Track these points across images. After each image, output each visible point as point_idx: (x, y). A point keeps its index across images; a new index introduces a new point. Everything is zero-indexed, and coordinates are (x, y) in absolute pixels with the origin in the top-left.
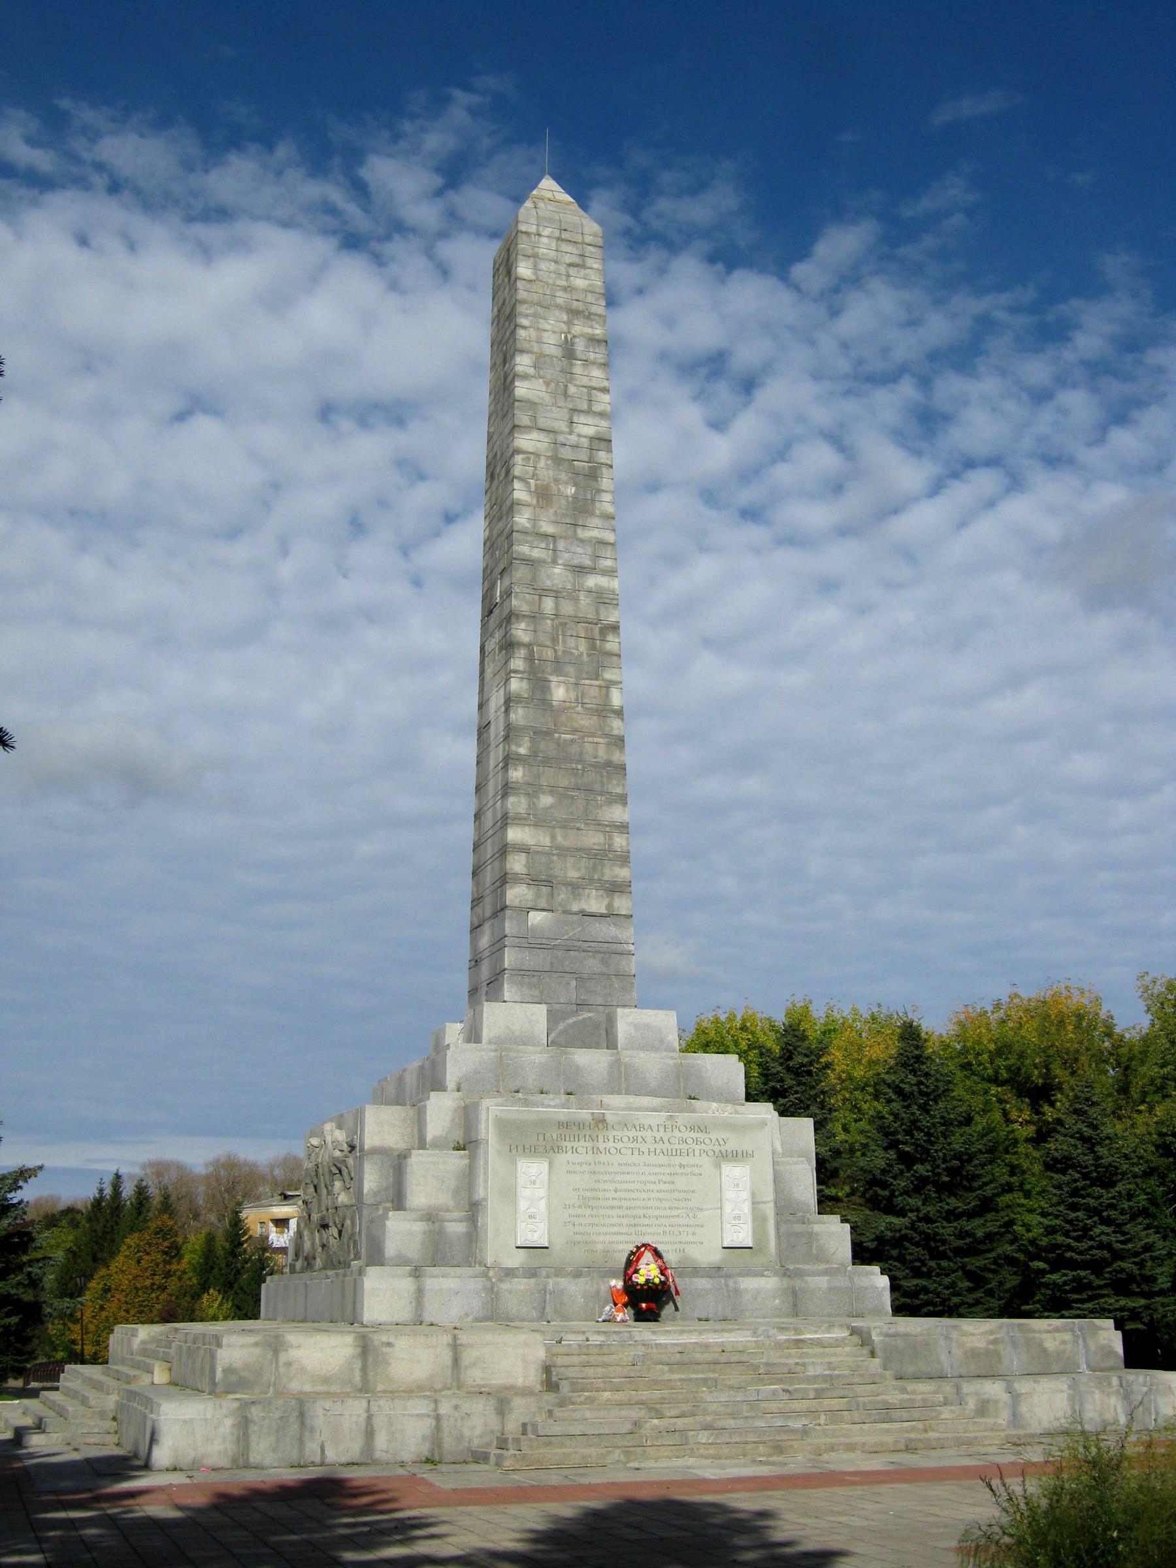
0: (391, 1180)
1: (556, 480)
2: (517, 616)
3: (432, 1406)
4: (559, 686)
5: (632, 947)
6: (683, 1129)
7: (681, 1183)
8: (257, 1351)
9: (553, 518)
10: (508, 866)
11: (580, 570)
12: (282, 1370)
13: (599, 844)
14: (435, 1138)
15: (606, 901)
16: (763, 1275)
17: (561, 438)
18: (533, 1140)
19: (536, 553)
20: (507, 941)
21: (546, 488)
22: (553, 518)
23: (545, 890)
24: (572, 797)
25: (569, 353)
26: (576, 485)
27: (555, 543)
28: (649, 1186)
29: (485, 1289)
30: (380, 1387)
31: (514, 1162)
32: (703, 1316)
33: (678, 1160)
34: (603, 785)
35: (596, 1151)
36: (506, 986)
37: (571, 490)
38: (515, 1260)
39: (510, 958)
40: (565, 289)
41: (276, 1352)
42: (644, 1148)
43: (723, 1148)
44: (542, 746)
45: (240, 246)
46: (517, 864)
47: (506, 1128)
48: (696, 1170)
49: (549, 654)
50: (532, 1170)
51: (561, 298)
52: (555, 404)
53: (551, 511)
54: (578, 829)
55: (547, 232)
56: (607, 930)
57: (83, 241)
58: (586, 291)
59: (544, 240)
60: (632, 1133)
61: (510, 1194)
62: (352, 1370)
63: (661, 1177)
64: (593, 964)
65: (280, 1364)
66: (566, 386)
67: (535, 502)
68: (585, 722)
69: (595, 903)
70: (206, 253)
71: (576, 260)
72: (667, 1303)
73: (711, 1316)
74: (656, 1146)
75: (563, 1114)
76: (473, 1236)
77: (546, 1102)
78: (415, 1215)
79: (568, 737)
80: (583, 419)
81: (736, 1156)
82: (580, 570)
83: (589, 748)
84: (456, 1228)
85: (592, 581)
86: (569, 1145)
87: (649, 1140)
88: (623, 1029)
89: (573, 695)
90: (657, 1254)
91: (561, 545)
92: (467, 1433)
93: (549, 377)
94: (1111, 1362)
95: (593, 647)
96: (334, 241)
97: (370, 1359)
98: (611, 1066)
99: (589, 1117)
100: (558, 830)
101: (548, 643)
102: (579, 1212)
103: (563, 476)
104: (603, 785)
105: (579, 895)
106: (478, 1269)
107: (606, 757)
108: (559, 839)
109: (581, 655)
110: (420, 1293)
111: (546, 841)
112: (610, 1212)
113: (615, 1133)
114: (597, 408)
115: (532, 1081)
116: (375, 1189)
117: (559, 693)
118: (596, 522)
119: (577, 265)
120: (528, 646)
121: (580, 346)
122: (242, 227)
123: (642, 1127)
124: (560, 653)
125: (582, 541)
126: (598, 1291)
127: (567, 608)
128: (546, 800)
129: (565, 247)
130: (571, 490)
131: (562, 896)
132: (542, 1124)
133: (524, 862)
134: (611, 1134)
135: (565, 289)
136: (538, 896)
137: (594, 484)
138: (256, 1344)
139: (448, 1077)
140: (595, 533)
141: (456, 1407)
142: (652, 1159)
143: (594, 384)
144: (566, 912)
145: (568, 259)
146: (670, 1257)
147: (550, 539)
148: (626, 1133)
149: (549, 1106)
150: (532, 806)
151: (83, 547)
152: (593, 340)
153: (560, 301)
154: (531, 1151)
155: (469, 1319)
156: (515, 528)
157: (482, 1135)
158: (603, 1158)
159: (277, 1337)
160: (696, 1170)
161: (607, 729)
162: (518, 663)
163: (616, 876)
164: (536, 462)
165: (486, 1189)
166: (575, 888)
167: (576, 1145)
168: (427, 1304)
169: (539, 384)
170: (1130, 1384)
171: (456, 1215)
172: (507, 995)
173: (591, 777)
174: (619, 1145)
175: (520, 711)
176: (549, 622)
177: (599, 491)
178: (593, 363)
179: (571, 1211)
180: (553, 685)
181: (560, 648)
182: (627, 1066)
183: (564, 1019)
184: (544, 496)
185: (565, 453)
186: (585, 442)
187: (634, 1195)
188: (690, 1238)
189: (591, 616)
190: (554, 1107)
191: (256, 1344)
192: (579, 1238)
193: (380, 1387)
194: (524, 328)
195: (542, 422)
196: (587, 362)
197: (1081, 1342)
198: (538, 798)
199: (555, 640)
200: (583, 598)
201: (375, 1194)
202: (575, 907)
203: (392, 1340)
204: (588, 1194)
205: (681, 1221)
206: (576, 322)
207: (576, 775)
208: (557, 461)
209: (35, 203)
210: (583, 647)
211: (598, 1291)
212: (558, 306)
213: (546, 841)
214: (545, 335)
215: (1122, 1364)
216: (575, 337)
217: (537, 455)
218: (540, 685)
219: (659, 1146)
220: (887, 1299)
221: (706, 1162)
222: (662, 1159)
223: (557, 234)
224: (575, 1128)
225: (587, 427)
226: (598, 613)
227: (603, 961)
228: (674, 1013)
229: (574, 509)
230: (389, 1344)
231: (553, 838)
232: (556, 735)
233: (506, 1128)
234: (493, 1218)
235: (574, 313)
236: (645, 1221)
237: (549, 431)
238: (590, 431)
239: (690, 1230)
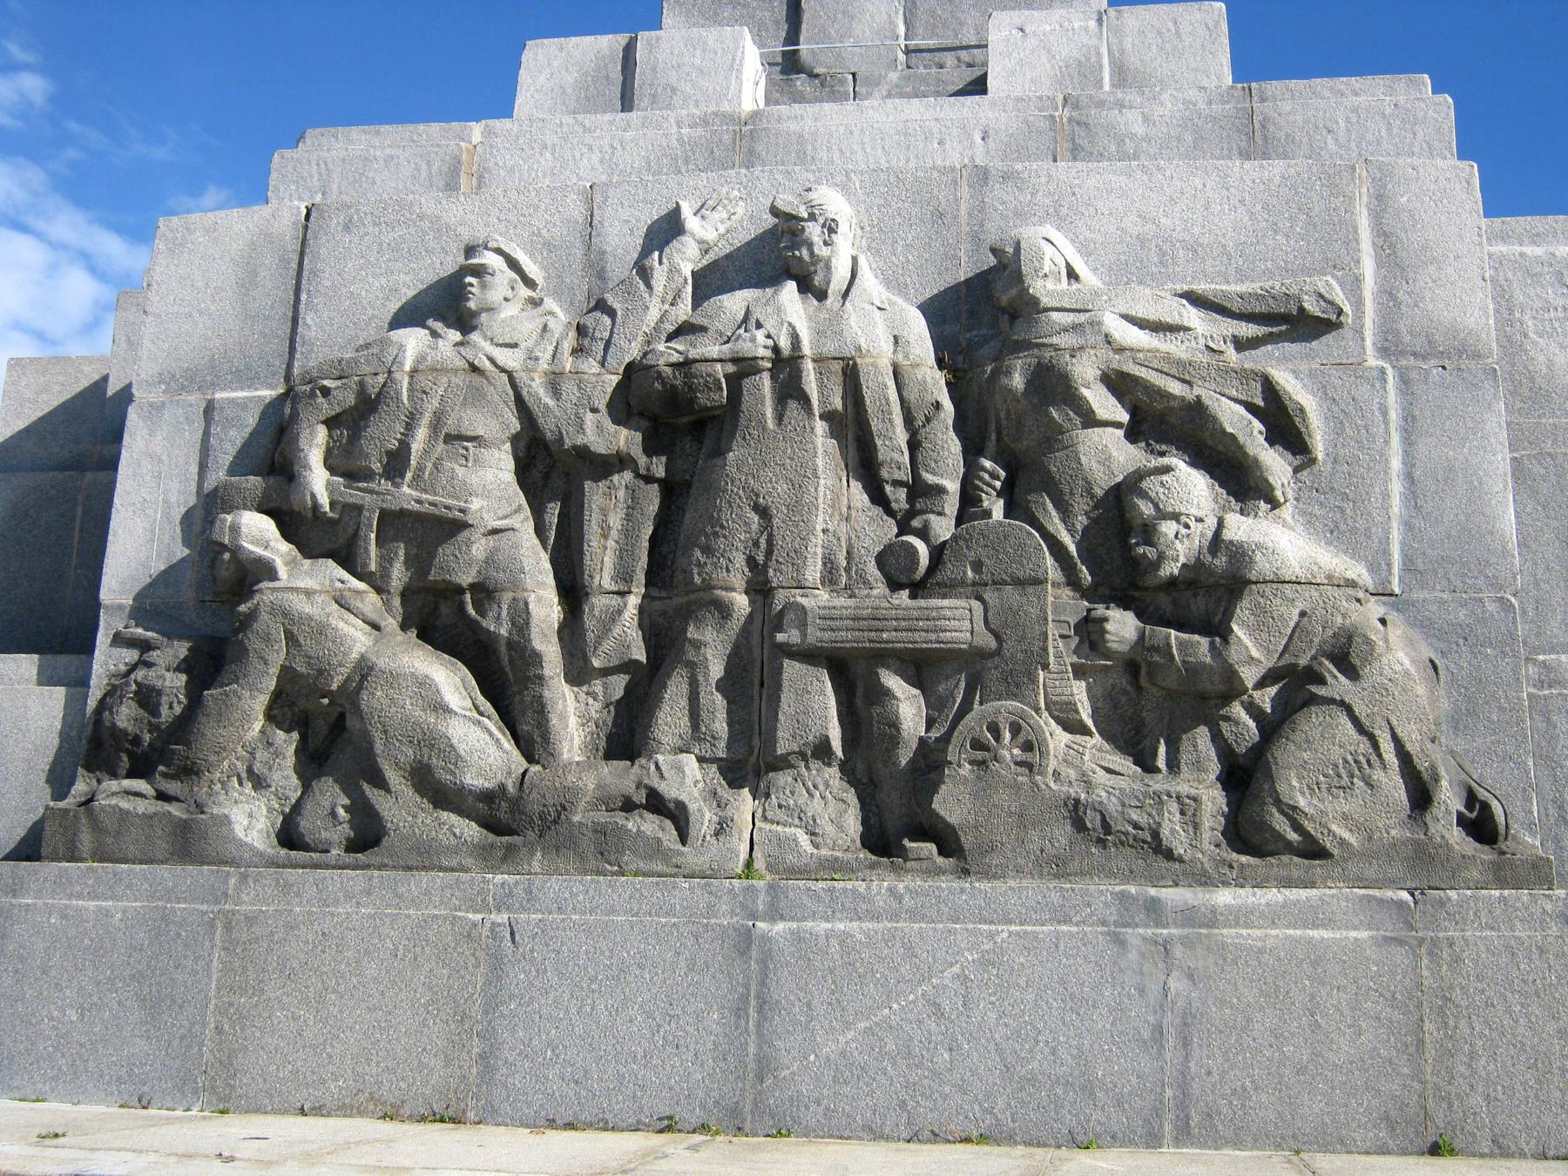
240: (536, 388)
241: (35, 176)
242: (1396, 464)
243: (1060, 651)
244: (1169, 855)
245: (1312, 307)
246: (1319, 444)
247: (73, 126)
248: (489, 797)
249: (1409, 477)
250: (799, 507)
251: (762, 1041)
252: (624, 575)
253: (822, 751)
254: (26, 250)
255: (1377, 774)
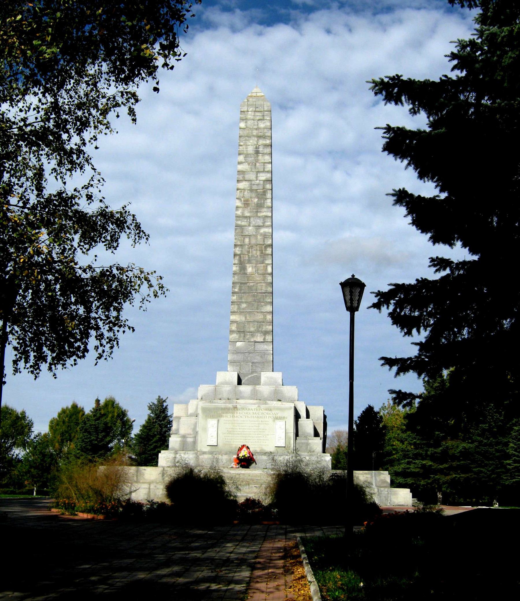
1: (251, 197)
3: (148, 486)
7: (262, 426)
9: (249, 210)
11: (258, 227)
15: (263, 337)
17: (253, 182)
19: (243, 224)
21: (247, 200)
23: (242, 335)
25: (257, 152)
26: (258, 198)
28: (251, 428)
30: (141, 481)
31: (206, 419)
33: (260, 420)
35: (233, 417)
37: (256, 200)
38: (207, 449)
40: (256, 129)
42: (249, 416)
44: (243, 288)
45: (400, 21)
48: (267, 423)
51: (255, 133)
52: (251, 171)
53: (249, 208)
55: (251, 110)
57: (328, 31)
58: (264, 128)
59: (250, 113)
60: (246, 411)
61: (205, 429)
66: (255, 164)
70: (384, 28)
71: (261, 118)
72: (253, 463)
75: (223, 406)
76: (195, 443)
78: (179, 436)
80: (261, 174)
81: (281, 418)
82: (258, 227)
83: (259, 287)
84: (190, 440)
85: (262, 231)
86: (225, 415)
88: (263, 379)
89: (254, 270)
90: (248, 448)
91: (252, 219)
92: (157, 493)
93: (249, 161)
94: (385, 485)
95: (262, 253)
96: (442, 11)
97: (139, 474)
99: (232, 407)
102: (227, 435)
106: (196, 452)
108: (248, 318)
111: (243, 319)
112: (238, 435)
114: (266, 170)
115: (225, 395)
117: (250, 269)
118: (265, 210)
121: (261, 149)
122: (398, 14)
123: (249, 409)
125: (259, 217)
126: (230, 459)
127: (253, 241)
128: (244, 306)
129: (257, 114)
130: (256, 200)
132: (217, 409)
134: (238, 412)
135: (256, 129)
136: (240, 337)
137: (264, 197)
140: (264, 214)
141: (155, 486)
142: (252, 419)
143: (266, 161)
145: (258, 118)
146: (251, 450)
151: (335, 168)
152: (266, 146)
153: (255, 134)
154: (213, 417)
158: (235, 419)
160: (267, 423)
164: (244, 192)
166: (253, 334)
167: (227, 415)
170: (382, 491)
171: (191, 436)
172: (229, 369)
177: (266, 199)
178: (266, 154)
179: (225, 435)
180: (247, 267)
181: (250, 255)
182: (257, 390)
183: (247, 376)
185: (255, 187)
186: (262, 182)
188: (264, 444)
189: (262, 243)
193: (141, 481)
195: (246, 179)
196: (264, 154)
197: (374, 478)
199: (249, 252)
200: (259, 237)
204: (231, 430)
208: (251, 190)
209: (307, 20)
210: (258, 253)
211: (230, 459)
212: (254, 136)
213: (243, 319)
214: (249, 147)
215: (389, 486)
217: (244, 190)
219: (254, 415)
221: (271, 420)
222: (256, 419)
223: (254, 109)
225: (263, 177)
226: (264, 241)
228: (281, 373)
229: (257, 206)
230: (145, 470)
231: (246, 318)
235: (259, 137)
236: (250, 438)
237: (249, 181)
238: (264, 178)
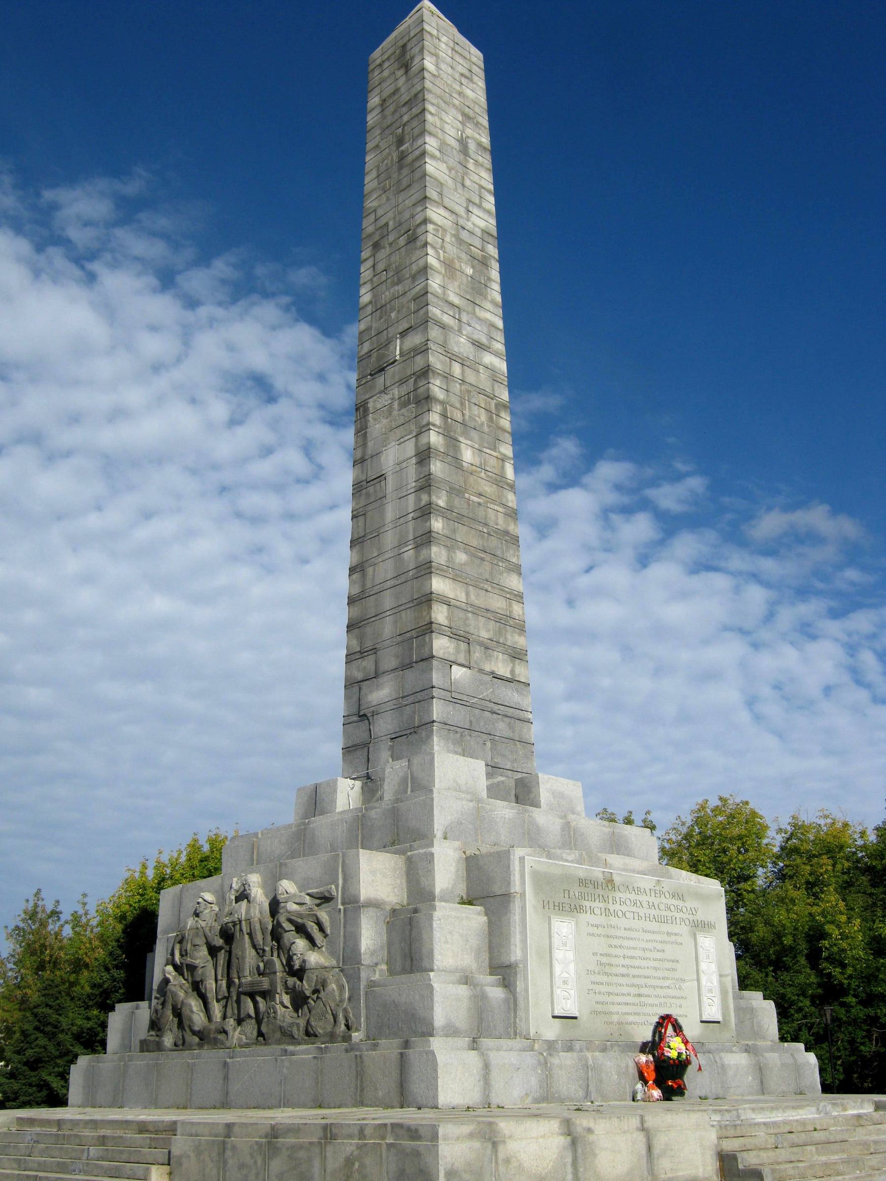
0: (385, 938)
2: (433, 372)
4: (467, 449)
5: (530, 716)
6: (667, 895)
8: (477, 1144)
10: (433, 616)
12: (502, 1169)
13: (502, 609)
14: (442, 890)
16: (732, 1052)
18: (567, 897)
19: (446, 319)
20: (435, 692)
22: (457, 291)
23: (463, 646)
24: (482, 559)
26: (473, 267)
27: (459, 314)
29: (540, 1063)
32: (703, 1094)
33: (665, 928)
34: (503, 552)
35: (607, 912)
36: (435, 739)
38: (551, 1031)
39: (438, 709)
41: (495, 1145)
43: (695, 918)
46: (440, 614)
47: (542, 881)
49: (458, 416)
50: (564, 928)
54: (487, 591)
56: (510, 695)
60: (633, 896)
61: (548, 956)
62: (565, 1165)
63: (655, 945)
64: (501, 727)
65: (500, 1161)
67: (443, 271)
68: (489, 489)
69: (502, 668)
73: (709, 1095)
74: (650, 911)
77: (564, 856)
79: (476, 499)
87: (645, 904)
95: (491, 419)
98: (563, 830)
100: (471, 588)
101: (458, 405)
103: (464, 256)
104: (503, 552)
105: (490, 656)
107: (504, 526)
109: (483, 424)
110: (487, 1066)
111: (462, 597)
112: (621, 980)
113: (621, 895)
116: (372, 948)
117: (468, 455)
119: (466, 77)
120: (442, 403)
124: (467, 417)
130: (469, 271)
131: (477, 655)
133: (446, 614)
134: (618, 895)
137: (486, 271)
138: (471, 1136)
139: (436, 826)
144: (481, 671)
145: (460, 69)
147: (457, 309)
148: (629, 896)
149: (567, 861)
150: (450, 559)
153: (457, 102)
155: (530, 1099)
156: (430, 290)
157: (516, 887)
159: (490, 1124)
161: (504, 500)
162: (435, 418)
163: (516, 643)
165: (524, 949)
167: (593, 905)
168: (493, 1083)
169: (443, 167)
173: (494, 542)
174: (624, 908)
175: (438, 464)
176: (458, 386)
180: (463, 446)
181: (467, 412)
184: (449, 266)
185: (464, 235)
187: (637, 963)
190: (572, 862)
191: (471, 1136)
192: (599, 1007)
194: (431, 113)
198: (454, 552)
201: (373, 953)
202: (488, 668)
203: (591, 1125)
204: (605, 960)
205: (671, 992)
206: (468, 125)
207: (483, 537)
213: (462, 597)
216: (468, 137)
218: (452, 442)
219: (652, 912)
220: (816, 1078)
221: (684, 929)
222: (654, 926)
224: (591, 886)
227: (511, 727)
232: (467, 495)
233: (542, 881)
234: (533, 982)
239: (678, 1002)
240: (207, 930)
241: (711, 535)
242: (342, 933)
243: (280, 988)
244: (293, 1037)
245: (327, 895)
246: (328, 931)
247: (726, 500)
248: (199, 1032)
249: (344, 936)
250: (243, 958)
251: (362, 1082)
252: (222, 976)
253: (249, 1016)
254: (720, 581)
255: (327, 1016)
